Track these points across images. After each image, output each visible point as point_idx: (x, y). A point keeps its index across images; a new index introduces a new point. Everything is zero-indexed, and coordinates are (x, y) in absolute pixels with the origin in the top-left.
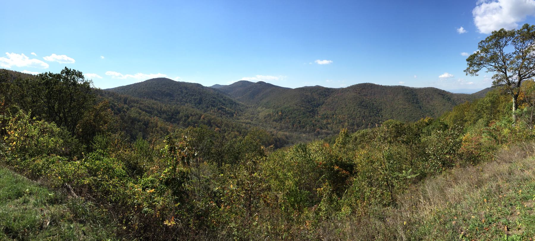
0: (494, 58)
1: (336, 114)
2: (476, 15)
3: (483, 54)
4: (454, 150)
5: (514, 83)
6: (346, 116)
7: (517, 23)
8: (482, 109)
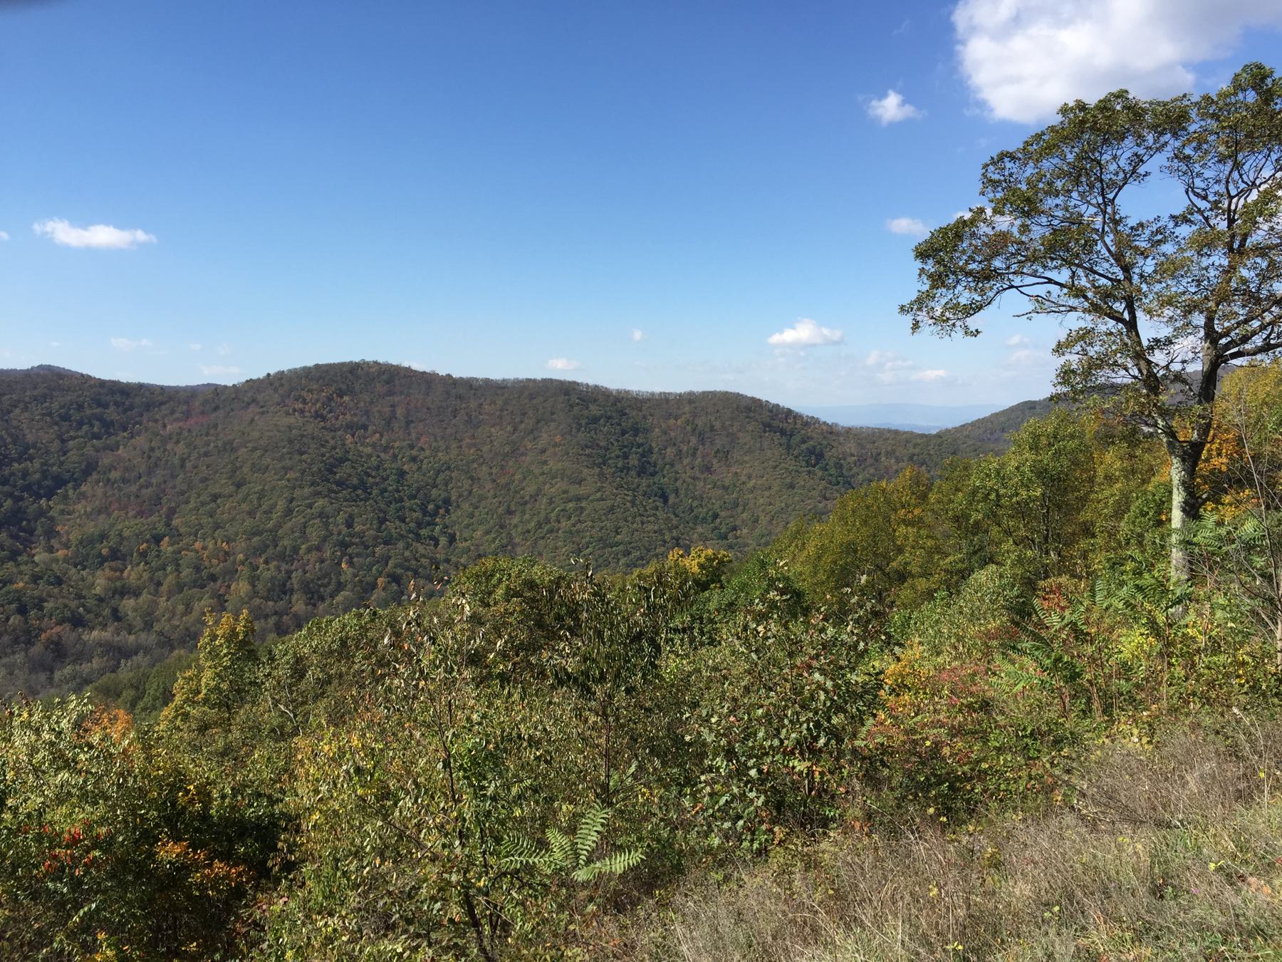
0: (1067, 245)
1: (176, 536)
2: (973, 30)
3: (1004, 223)
4: (836, 735)
5: (1178, 377)
6: (241, 545)
7: (1187, 65)
8: (993, 516)
